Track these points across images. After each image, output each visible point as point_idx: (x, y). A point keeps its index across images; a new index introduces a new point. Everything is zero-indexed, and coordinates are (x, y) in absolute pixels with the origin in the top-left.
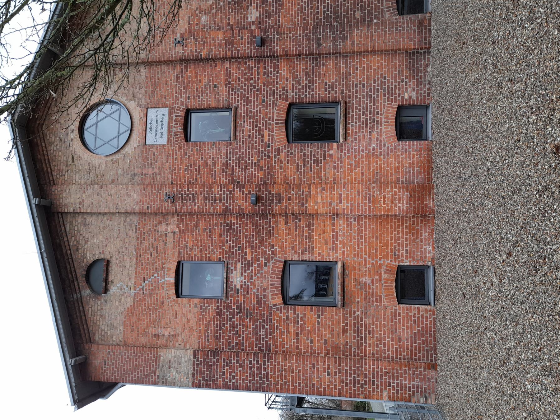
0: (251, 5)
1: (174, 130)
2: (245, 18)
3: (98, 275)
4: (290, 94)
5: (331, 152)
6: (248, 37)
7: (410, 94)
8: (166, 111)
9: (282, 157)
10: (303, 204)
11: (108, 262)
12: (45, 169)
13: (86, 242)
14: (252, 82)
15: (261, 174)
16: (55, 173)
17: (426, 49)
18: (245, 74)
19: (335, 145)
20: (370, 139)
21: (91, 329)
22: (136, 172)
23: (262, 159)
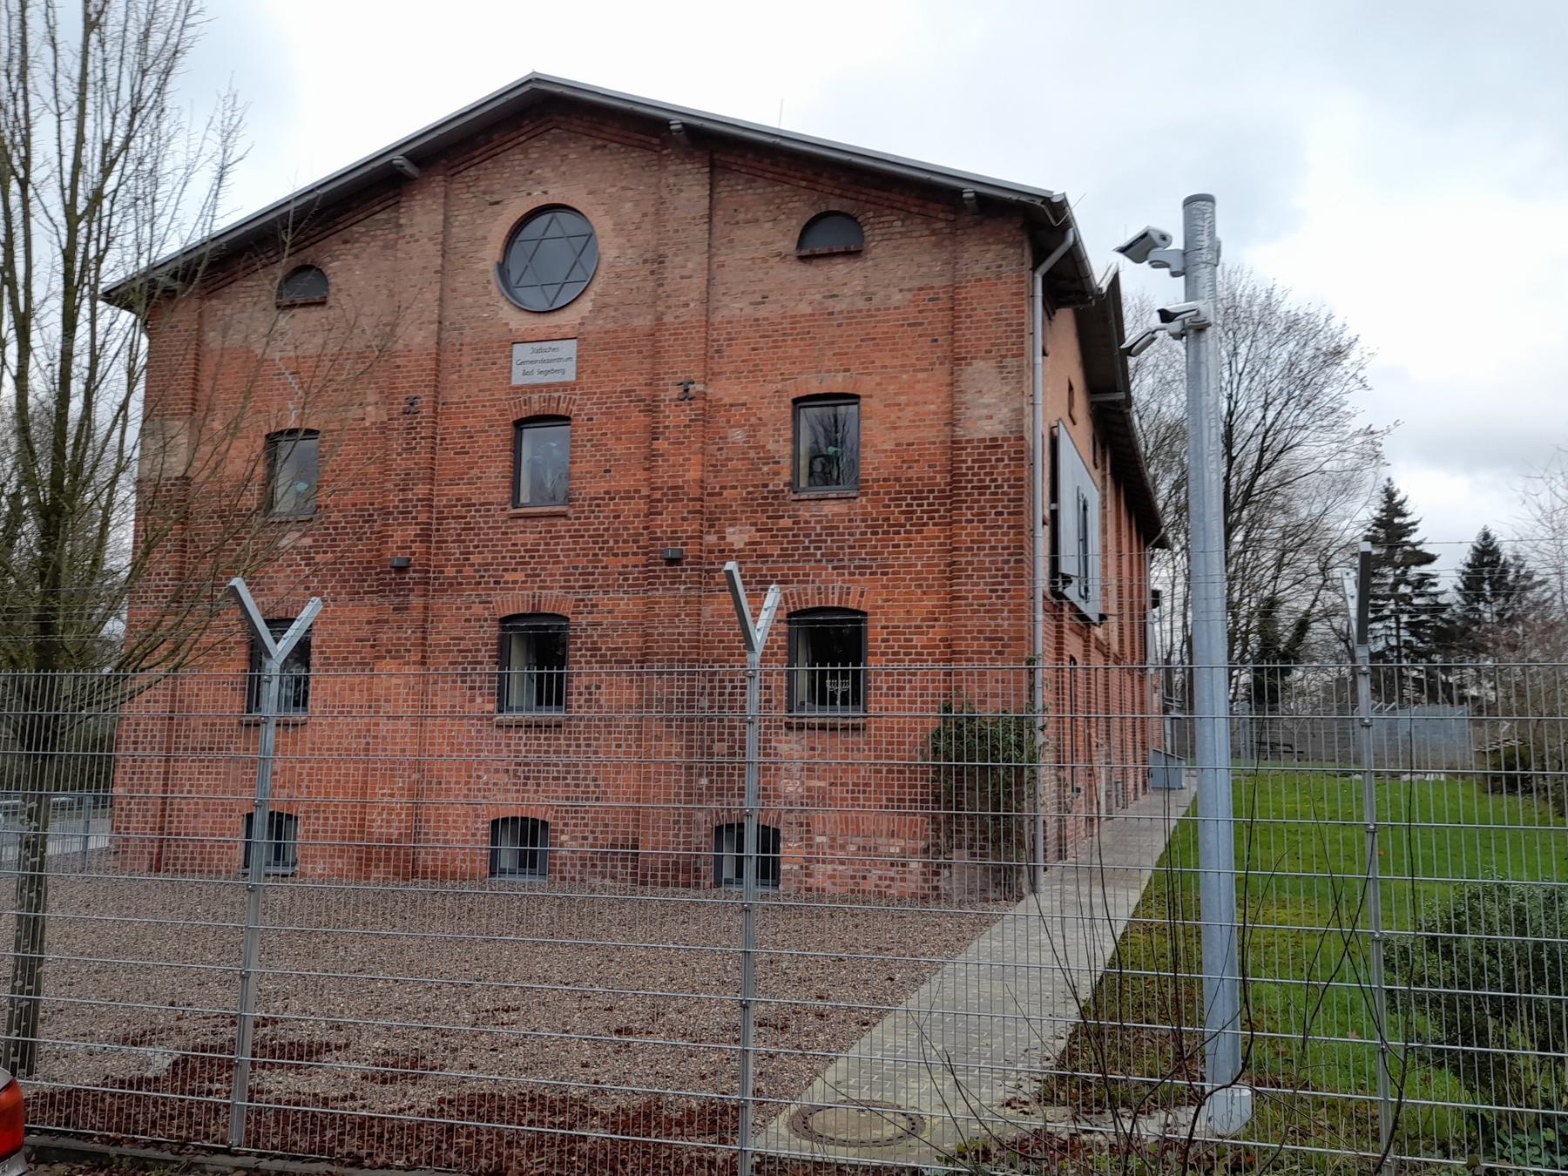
0: (758, 530)
1: (535, 397)
2: (734, 521)
3: (306, 287)
4: (583, 620)
5: (479, 700)
6: (685, 531)
7: (566, 845)
8: (570, 376)
9: (477, 609)
10: (389, 651)
11: (322, 303)
12: (476, 153)
13: (356, 257)
14: (611, 543)
15: (450, 571)
16: (472, 172)
17: (641, 879)
18: (626, 529)
19: (490, 707)
20: (497, 771)
21: (227, 290)
22: (467, 331)
23: (477, 571)
